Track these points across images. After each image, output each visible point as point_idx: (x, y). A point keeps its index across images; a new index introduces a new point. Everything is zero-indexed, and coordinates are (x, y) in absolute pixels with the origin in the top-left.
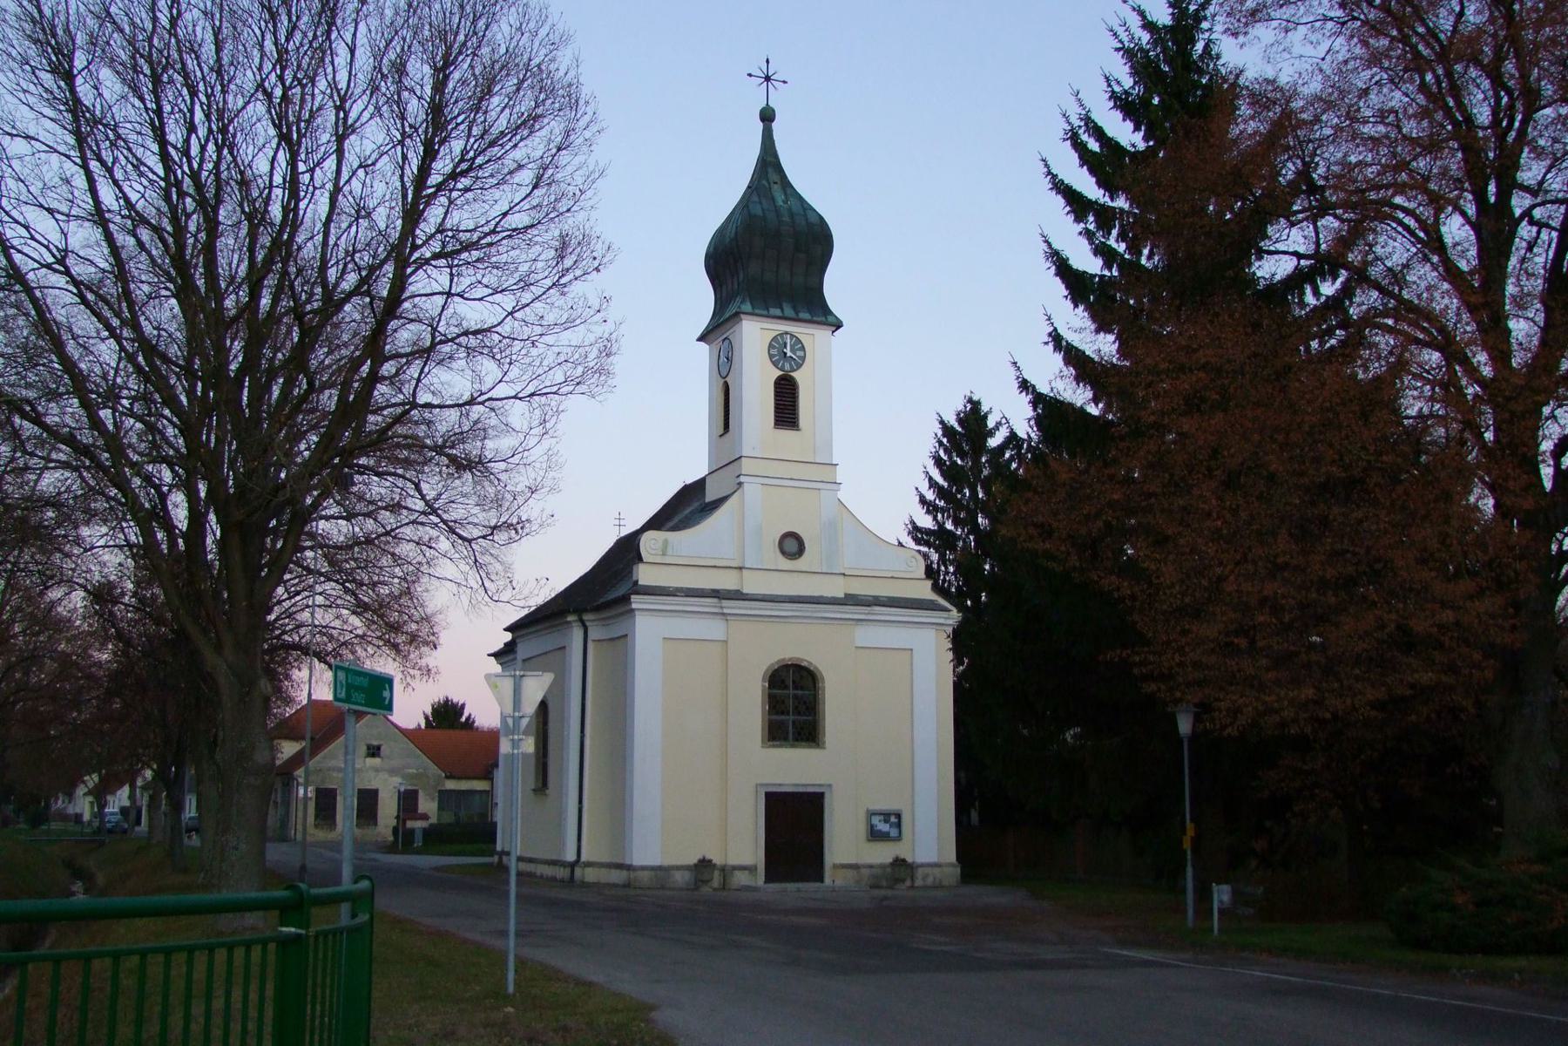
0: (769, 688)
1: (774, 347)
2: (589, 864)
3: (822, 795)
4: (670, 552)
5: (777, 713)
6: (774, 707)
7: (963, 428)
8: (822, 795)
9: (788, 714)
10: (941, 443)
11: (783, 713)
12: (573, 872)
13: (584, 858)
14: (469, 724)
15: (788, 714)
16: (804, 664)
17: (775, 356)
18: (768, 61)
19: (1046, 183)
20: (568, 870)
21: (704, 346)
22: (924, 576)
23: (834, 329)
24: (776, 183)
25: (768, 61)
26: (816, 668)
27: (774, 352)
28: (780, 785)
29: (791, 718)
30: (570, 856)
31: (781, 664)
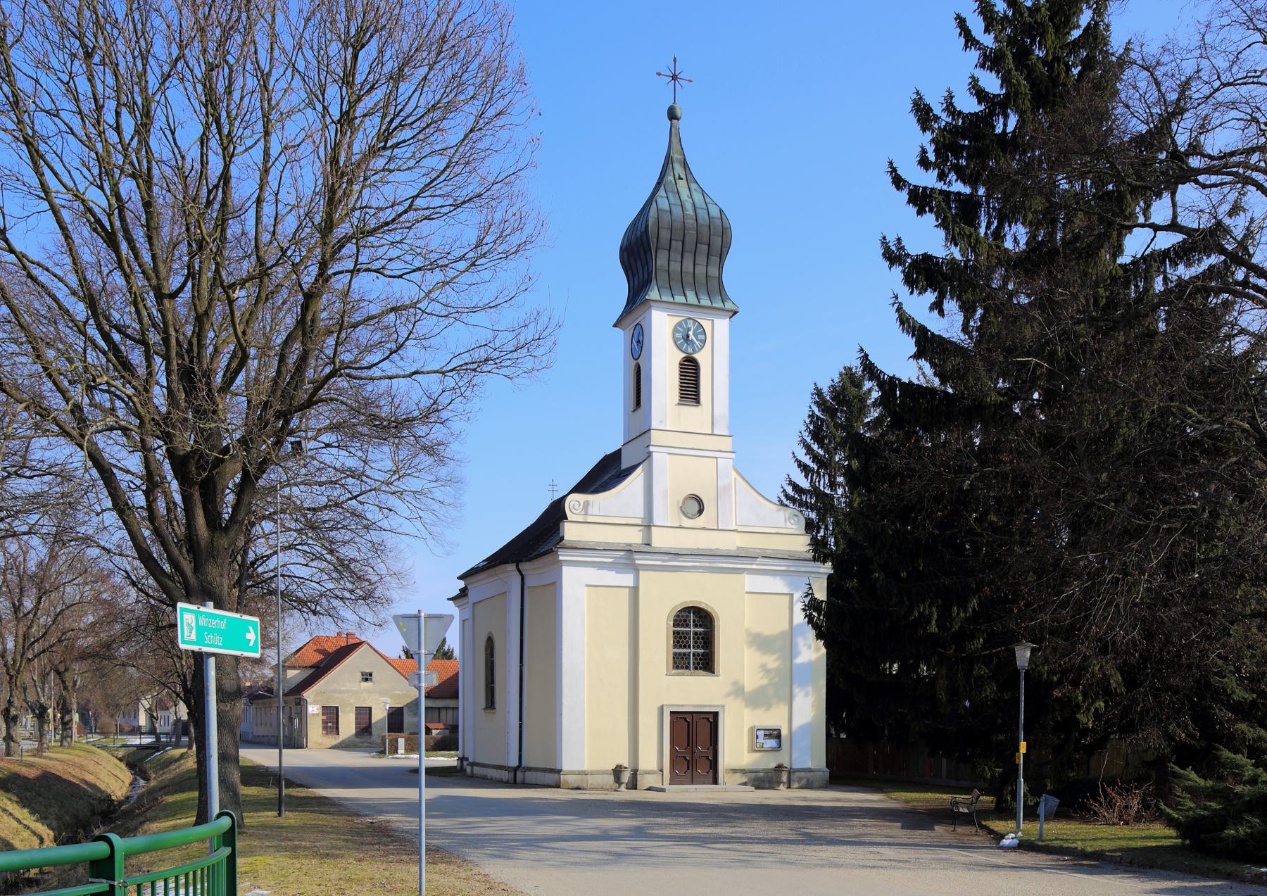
0: (674, 626)
1: (679, 332)
2: (530, 769)
3: (716, 714)
5: (680, 647)
6: (678, 642)
8: (716, 714)
13: (524, 764)
15: (689, 647)
17: (679, 339)
18: (675, 60)
24: (680, 178)
25: (675, 60)
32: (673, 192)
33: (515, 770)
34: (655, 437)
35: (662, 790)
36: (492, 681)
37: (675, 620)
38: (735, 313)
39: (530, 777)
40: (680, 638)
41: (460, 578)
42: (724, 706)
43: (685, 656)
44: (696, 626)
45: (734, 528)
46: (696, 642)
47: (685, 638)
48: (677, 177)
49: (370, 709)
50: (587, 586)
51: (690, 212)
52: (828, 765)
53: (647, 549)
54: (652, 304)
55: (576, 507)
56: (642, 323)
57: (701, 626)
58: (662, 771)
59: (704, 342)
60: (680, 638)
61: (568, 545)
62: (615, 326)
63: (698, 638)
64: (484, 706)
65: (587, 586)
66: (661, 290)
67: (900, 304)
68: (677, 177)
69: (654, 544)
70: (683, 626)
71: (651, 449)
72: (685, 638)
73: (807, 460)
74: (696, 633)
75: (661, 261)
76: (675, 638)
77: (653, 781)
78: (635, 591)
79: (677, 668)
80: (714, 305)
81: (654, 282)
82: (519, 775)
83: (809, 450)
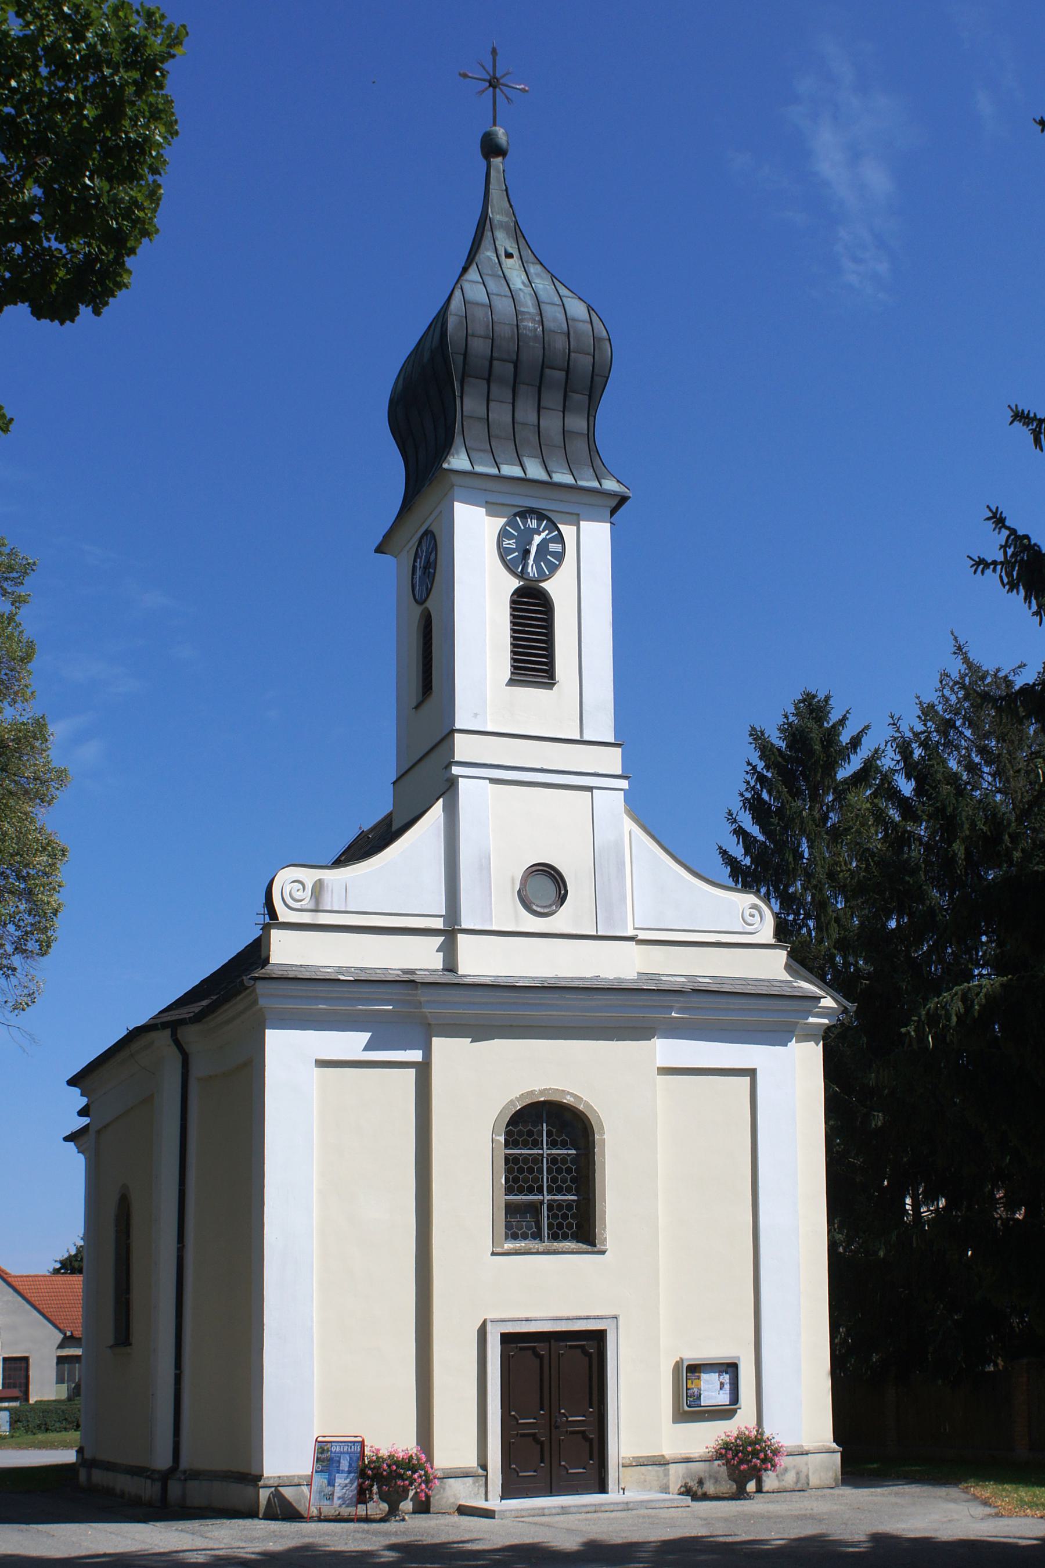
0: (507, 1145)
1: (510, 536)
2: (195, 1475)
3: (599, 1337)
4: (327, 904)
5: (521, 1191)
6: (516, 1180)
7: (764, 830)
8: (599, 1337)
9: (540, 1191)
10: (761, 779)
11: (530, 1191)
12: (165, 1489)
13: (185, 1464)
14: (79, 1250)
15: (540, 1191)
16: (568, 1100)
17: (510, 551)
18: (494, 52)
19: (719, 859)
20: (158, 1486)
21: (387, 560)
22: (773, 941)
23: (613, 503)
24: (509, 256)
25: (494, 52)
26: (587, 1104)
27: (509, 543)
28: (527, 1320)
29: (546, 1152)
30: (162, 1461)
31: (529, 1101)
32: (494, 275)
33: (165, 1477)
34: (464, 748)
35: (488, 1514)
36: (128, 1290)
37: (508, 1134)
38: (623, 500)
39: (197, 1492)
40: (521, 1170)
41: (72, 1082)
42: (616, 1318)
43: (534, 1209)
44: (552, 1144)
45: (630, 933)
46: (554, 1180)
47: (531, 1171)
48: (502, 253)
49: (5, 1359)
50: (322, 1064)
51: (528, 306)
52: (839, 1436)
53: (449, 978)
54: (455, 479)
55: (298, 895)
56: (435, 529)
57: (564, 1145)
58: (484, 1467)
59: (560, 556)
60: (521, 1170)
61: (277, 973)
62: (379, 550)
63: (559, 1171)
64: (111, 1341)
65: (322, 1064)
66: (473, 454)
67: (725, 851)
68: (502, 253)
69: (461, 971)
70: (525, 1145)
71: (456, 770)
72: (531, 1171)
73: (737, 851)
74: (553, 1160)
75: (471, 404)
76: (508, 1171)
77: (463, 1492)
78: (423, 1071)
79: (515, 1237)
80: (581, 483)
81: (458, 440)
82: (175, 1489)
83: (740, 832)
